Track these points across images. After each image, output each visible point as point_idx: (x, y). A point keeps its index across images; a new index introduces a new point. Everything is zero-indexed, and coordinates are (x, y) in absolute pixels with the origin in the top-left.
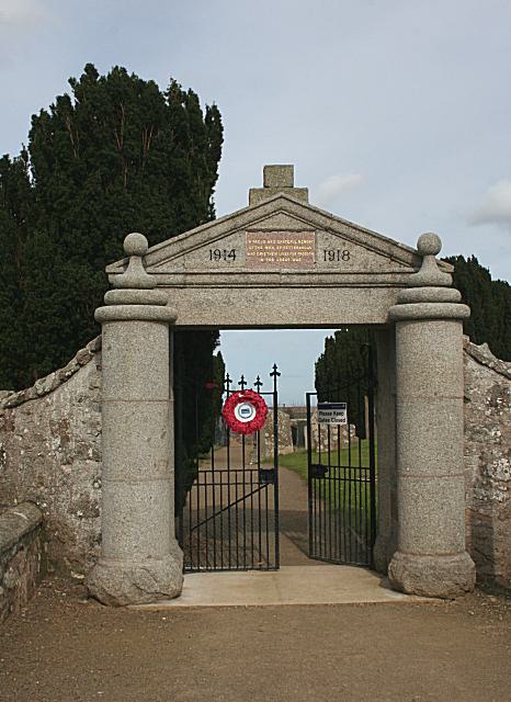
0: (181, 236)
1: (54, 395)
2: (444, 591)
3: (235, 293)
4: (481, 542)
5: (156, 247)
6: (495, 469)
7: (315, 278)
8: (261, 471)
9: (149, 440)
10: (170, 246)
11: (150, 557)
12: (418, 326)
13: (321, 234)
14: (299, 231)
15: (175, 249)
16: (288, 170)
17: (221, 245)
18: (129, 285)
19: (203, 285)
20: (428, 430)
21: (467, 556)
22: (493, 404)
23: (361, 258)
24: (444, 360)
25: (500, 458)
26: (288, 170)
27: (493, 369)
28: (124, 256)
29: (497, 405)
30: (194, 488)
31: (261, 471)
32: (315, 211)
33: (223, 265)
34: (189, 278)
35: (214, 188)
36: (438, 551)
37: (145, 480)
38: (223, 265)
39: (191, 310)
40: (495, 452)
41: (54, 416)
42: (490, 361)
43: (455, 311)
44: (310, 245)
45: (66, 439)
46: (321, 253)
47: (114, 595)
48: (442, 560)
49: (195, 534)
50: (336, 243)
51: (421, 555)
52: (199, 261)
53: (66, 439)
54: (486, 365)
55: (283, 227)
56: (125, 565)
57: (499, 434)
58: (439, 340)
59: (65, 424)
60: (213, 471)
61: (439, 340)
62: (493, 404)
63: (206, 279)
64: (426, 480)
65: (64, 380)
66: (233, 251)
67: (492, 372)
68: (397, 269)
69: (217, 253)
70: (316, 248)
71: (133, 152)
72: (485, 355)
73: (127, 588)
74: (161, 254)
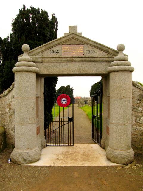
0: (41, 46)
1: (8, 96)
2: (125, 163)
3: (58, 64)
4: (135, 142)
5: (32, 50)
6: (140, 120)
7: (83, 59)
8: (69, 118)
9: (28, 111)
10: (38, 49)
11: (28, 149)
12: (117, 74)
13: (85, 45)
14: (79, 44)
15: (39, 50)
16: (76, 27)
17: (55, 49)
18: (23, 60)
19: (48, 62)
20: (120, 109)
21: (131, 150)
22: (139, 100)
23: (98, 54)
24: (126, 85)
25: (141, 116)
26: (76, 27)
27: (140, 88)
28: (21, 53)
29: (140, 100)
30: (52, 123)
31: (69, 118)
32: (84, 38)
33: (54, 55)
34: (44, 59)
35: (37, 9)
36: (123, 149)
37: (26, 124)
38: (54, 55)
39: (47, 69)
40: (140, 115)
41: (7, 102)
42: (139, 86)
43: (130, 68)
44: (82, 49)
45: (10, 109)
46: (85, 51)
47: (17, 161)
48: (123, 152)
49: (54, 134)
50: (90, 48)
51: (117, 150)
52: (48, 54)
53: (10, 109)
54: (137, 87)
55: (74, 43)
56: (20, 151)
57: (141, 109)
58: (125, 78)
59: (10, 104)
60: (59, 118)
61: (125, 78)
62: (139, 100)
63: (49, 59)
64: (119, 125)
65: (10, 91)
66: (58, 51)
67: (139, 90)
68: (109, 56)
69: (53, 51)
70: (84, 50)
71: (35, 28)
72: (137, 84)
73: (20, 159)
74: (35, 52)
